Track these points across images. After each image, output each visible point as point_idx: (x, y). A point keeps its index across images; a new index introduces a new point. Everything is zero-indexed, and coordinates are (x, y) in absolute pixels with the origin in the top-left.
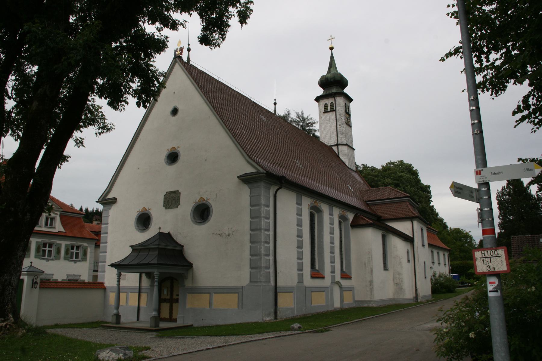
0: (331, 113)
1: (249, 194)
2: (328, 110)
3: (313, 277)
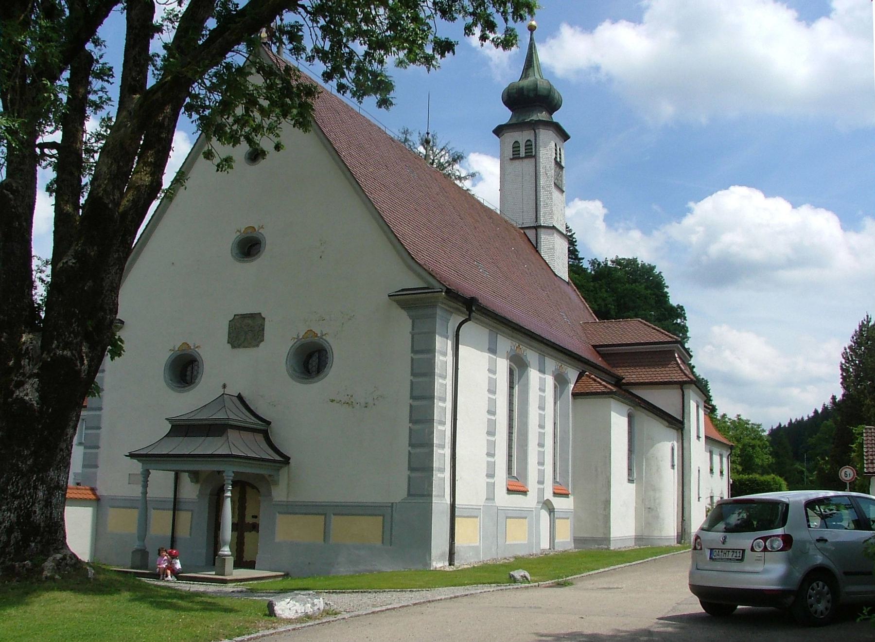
0: (526, 161)
1: (410, 329)
2: (521, 156)
3: (510, 491)
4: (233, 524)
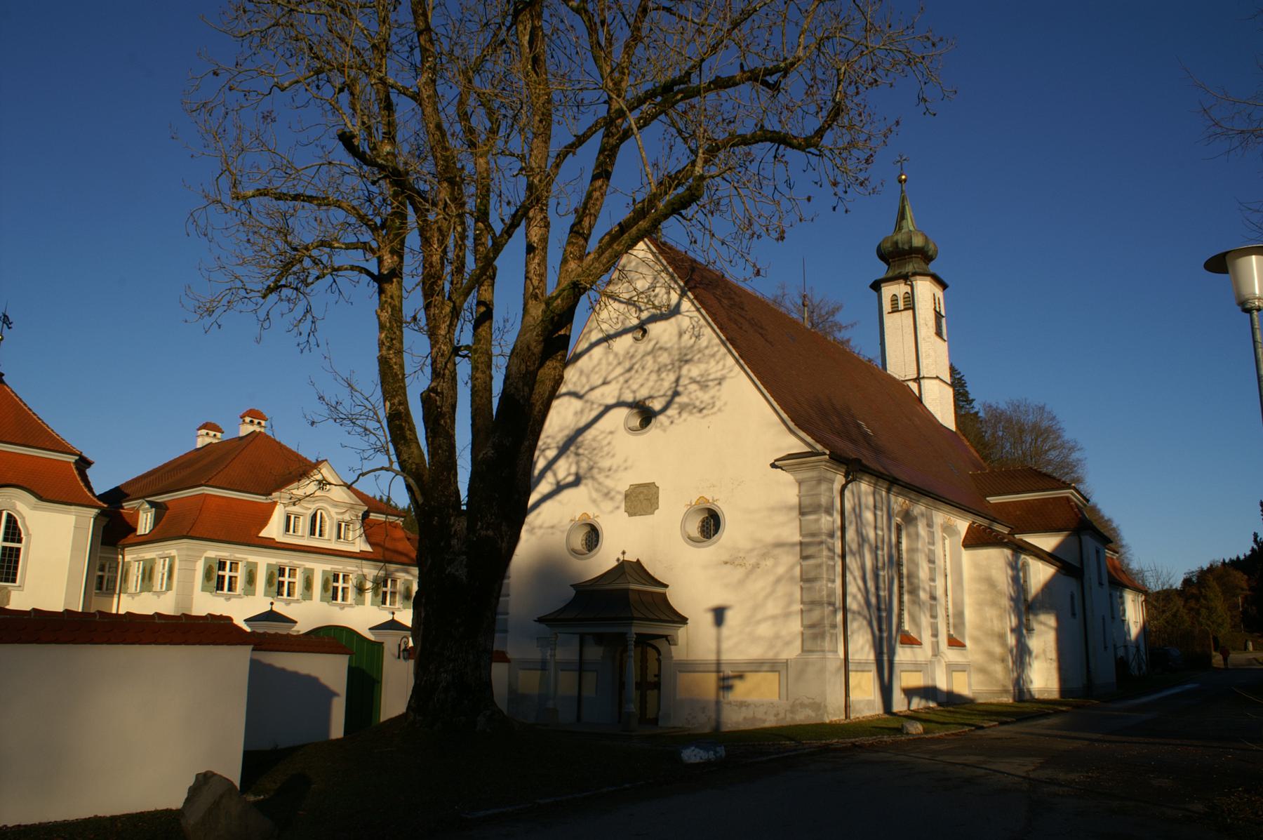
4: (636, 683)
